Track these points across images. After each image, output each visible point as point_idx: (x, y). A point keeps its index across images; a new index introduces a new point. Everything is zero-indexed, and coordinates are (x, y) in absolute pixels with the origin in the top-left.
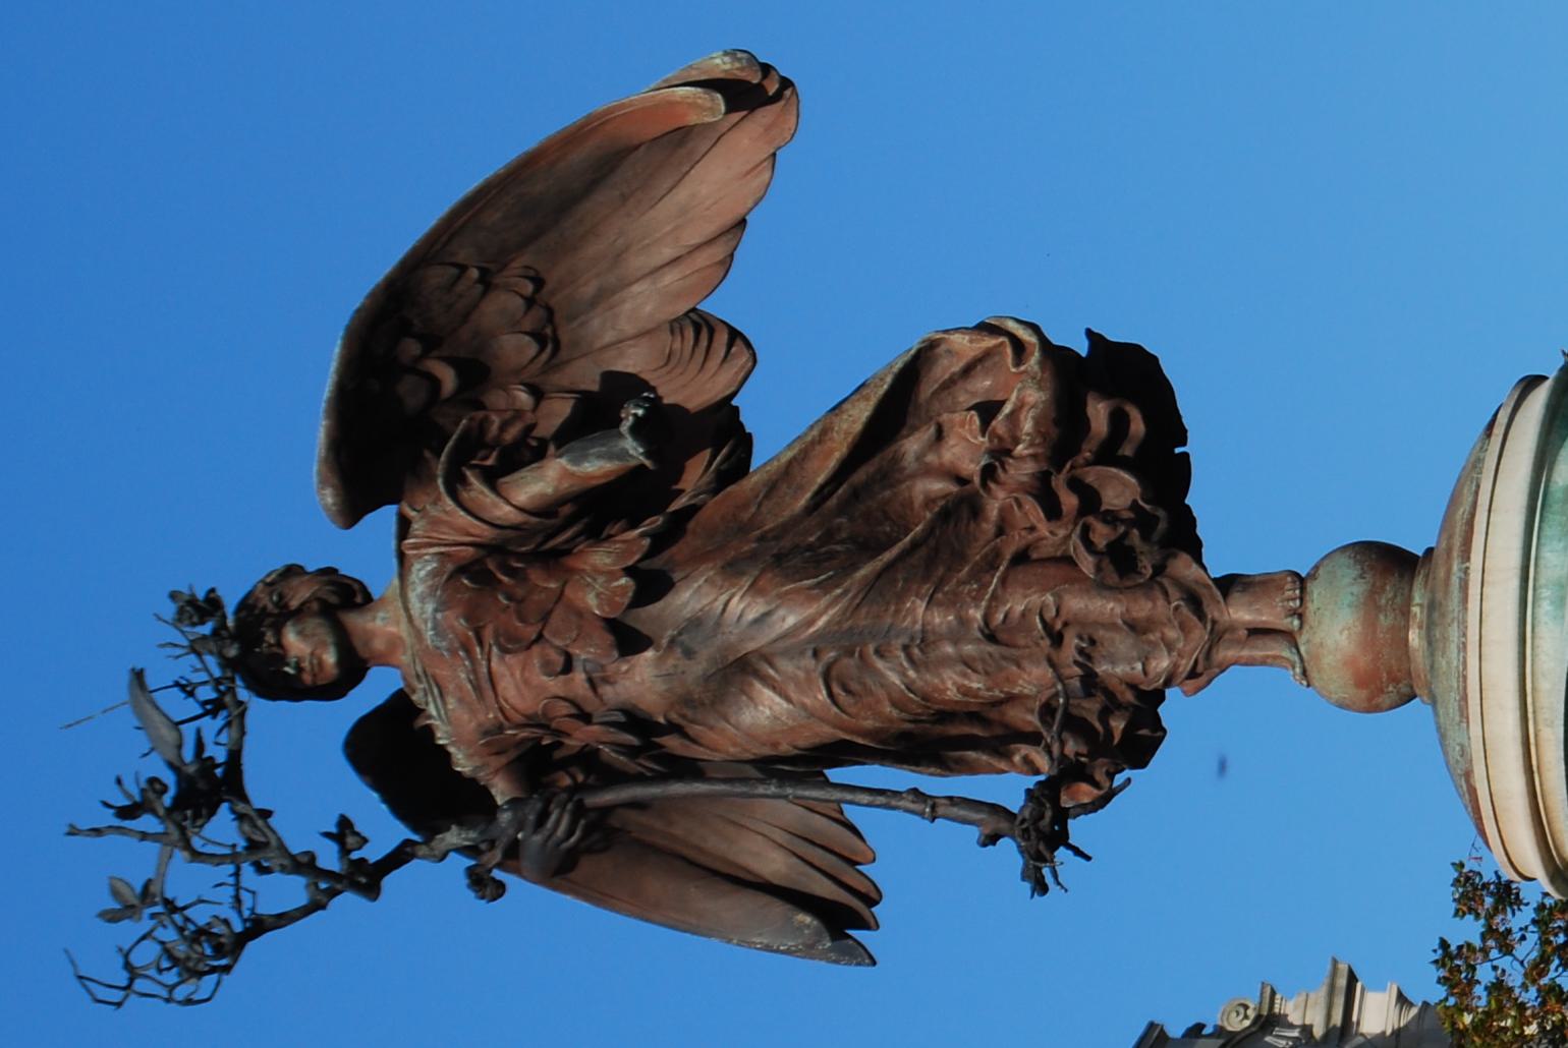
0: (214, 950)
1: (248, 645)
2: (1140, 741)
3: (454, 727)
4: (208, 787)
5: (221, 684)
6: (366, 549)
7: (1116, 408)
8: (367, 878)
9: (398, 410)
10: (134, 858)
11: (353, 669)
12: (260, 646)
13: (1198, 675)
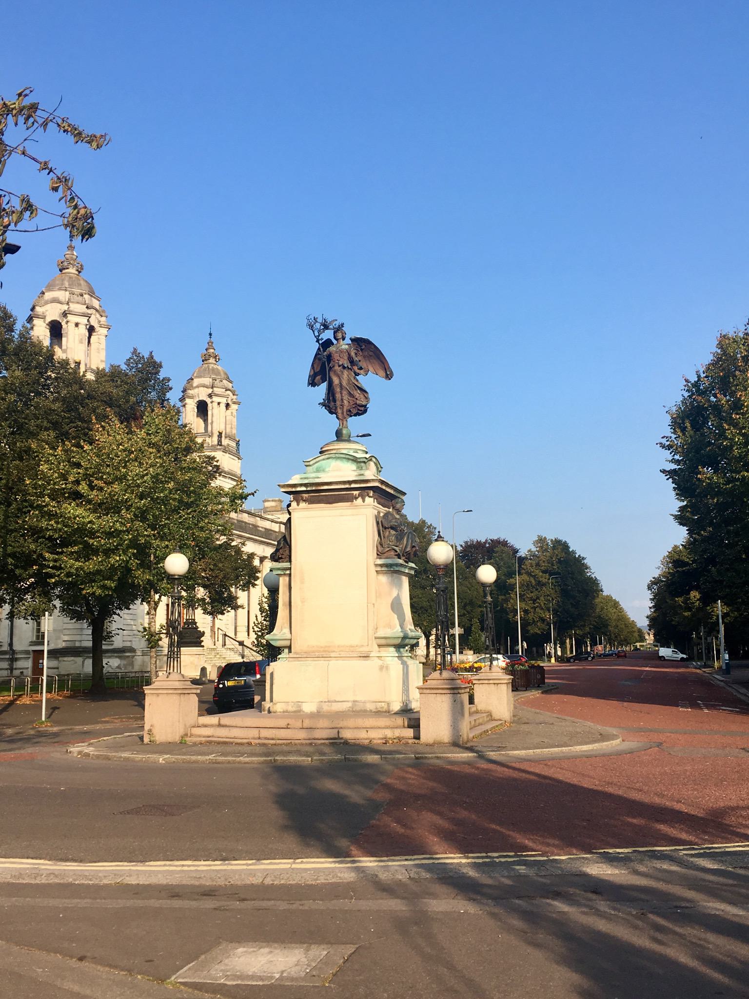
0: (311, 327)
1: (338, 329)
2: (331, 413)
3: (332, 349)
4: (326, 327)
5: (713, 462)
6: (348, 341)
7: (361, 410)
8: (318, 341)
9: (361, 344)
10: (320, 320)
11: (337, 340)
12: (711, 618)
13: (338, 418)
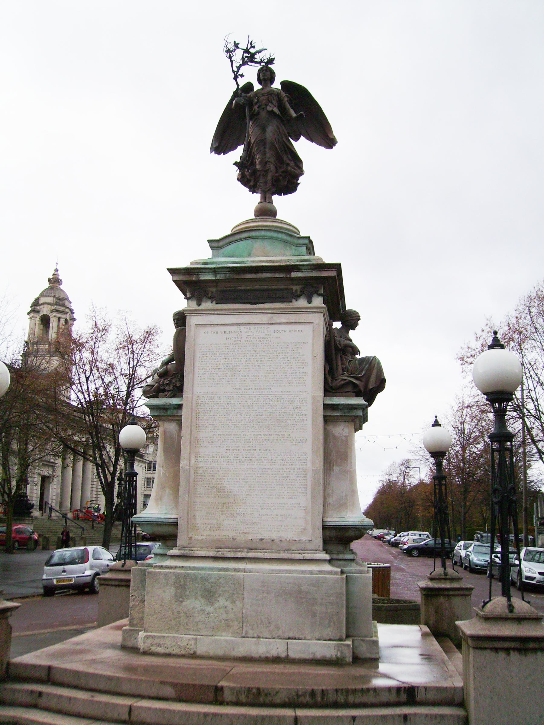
8: (235, 78)
